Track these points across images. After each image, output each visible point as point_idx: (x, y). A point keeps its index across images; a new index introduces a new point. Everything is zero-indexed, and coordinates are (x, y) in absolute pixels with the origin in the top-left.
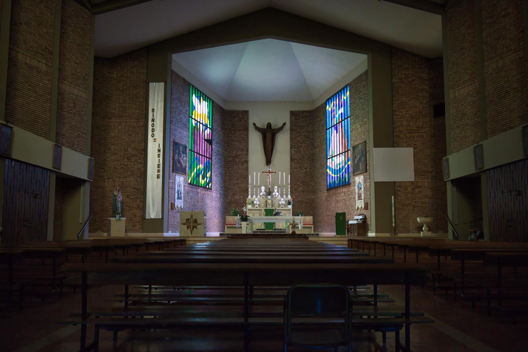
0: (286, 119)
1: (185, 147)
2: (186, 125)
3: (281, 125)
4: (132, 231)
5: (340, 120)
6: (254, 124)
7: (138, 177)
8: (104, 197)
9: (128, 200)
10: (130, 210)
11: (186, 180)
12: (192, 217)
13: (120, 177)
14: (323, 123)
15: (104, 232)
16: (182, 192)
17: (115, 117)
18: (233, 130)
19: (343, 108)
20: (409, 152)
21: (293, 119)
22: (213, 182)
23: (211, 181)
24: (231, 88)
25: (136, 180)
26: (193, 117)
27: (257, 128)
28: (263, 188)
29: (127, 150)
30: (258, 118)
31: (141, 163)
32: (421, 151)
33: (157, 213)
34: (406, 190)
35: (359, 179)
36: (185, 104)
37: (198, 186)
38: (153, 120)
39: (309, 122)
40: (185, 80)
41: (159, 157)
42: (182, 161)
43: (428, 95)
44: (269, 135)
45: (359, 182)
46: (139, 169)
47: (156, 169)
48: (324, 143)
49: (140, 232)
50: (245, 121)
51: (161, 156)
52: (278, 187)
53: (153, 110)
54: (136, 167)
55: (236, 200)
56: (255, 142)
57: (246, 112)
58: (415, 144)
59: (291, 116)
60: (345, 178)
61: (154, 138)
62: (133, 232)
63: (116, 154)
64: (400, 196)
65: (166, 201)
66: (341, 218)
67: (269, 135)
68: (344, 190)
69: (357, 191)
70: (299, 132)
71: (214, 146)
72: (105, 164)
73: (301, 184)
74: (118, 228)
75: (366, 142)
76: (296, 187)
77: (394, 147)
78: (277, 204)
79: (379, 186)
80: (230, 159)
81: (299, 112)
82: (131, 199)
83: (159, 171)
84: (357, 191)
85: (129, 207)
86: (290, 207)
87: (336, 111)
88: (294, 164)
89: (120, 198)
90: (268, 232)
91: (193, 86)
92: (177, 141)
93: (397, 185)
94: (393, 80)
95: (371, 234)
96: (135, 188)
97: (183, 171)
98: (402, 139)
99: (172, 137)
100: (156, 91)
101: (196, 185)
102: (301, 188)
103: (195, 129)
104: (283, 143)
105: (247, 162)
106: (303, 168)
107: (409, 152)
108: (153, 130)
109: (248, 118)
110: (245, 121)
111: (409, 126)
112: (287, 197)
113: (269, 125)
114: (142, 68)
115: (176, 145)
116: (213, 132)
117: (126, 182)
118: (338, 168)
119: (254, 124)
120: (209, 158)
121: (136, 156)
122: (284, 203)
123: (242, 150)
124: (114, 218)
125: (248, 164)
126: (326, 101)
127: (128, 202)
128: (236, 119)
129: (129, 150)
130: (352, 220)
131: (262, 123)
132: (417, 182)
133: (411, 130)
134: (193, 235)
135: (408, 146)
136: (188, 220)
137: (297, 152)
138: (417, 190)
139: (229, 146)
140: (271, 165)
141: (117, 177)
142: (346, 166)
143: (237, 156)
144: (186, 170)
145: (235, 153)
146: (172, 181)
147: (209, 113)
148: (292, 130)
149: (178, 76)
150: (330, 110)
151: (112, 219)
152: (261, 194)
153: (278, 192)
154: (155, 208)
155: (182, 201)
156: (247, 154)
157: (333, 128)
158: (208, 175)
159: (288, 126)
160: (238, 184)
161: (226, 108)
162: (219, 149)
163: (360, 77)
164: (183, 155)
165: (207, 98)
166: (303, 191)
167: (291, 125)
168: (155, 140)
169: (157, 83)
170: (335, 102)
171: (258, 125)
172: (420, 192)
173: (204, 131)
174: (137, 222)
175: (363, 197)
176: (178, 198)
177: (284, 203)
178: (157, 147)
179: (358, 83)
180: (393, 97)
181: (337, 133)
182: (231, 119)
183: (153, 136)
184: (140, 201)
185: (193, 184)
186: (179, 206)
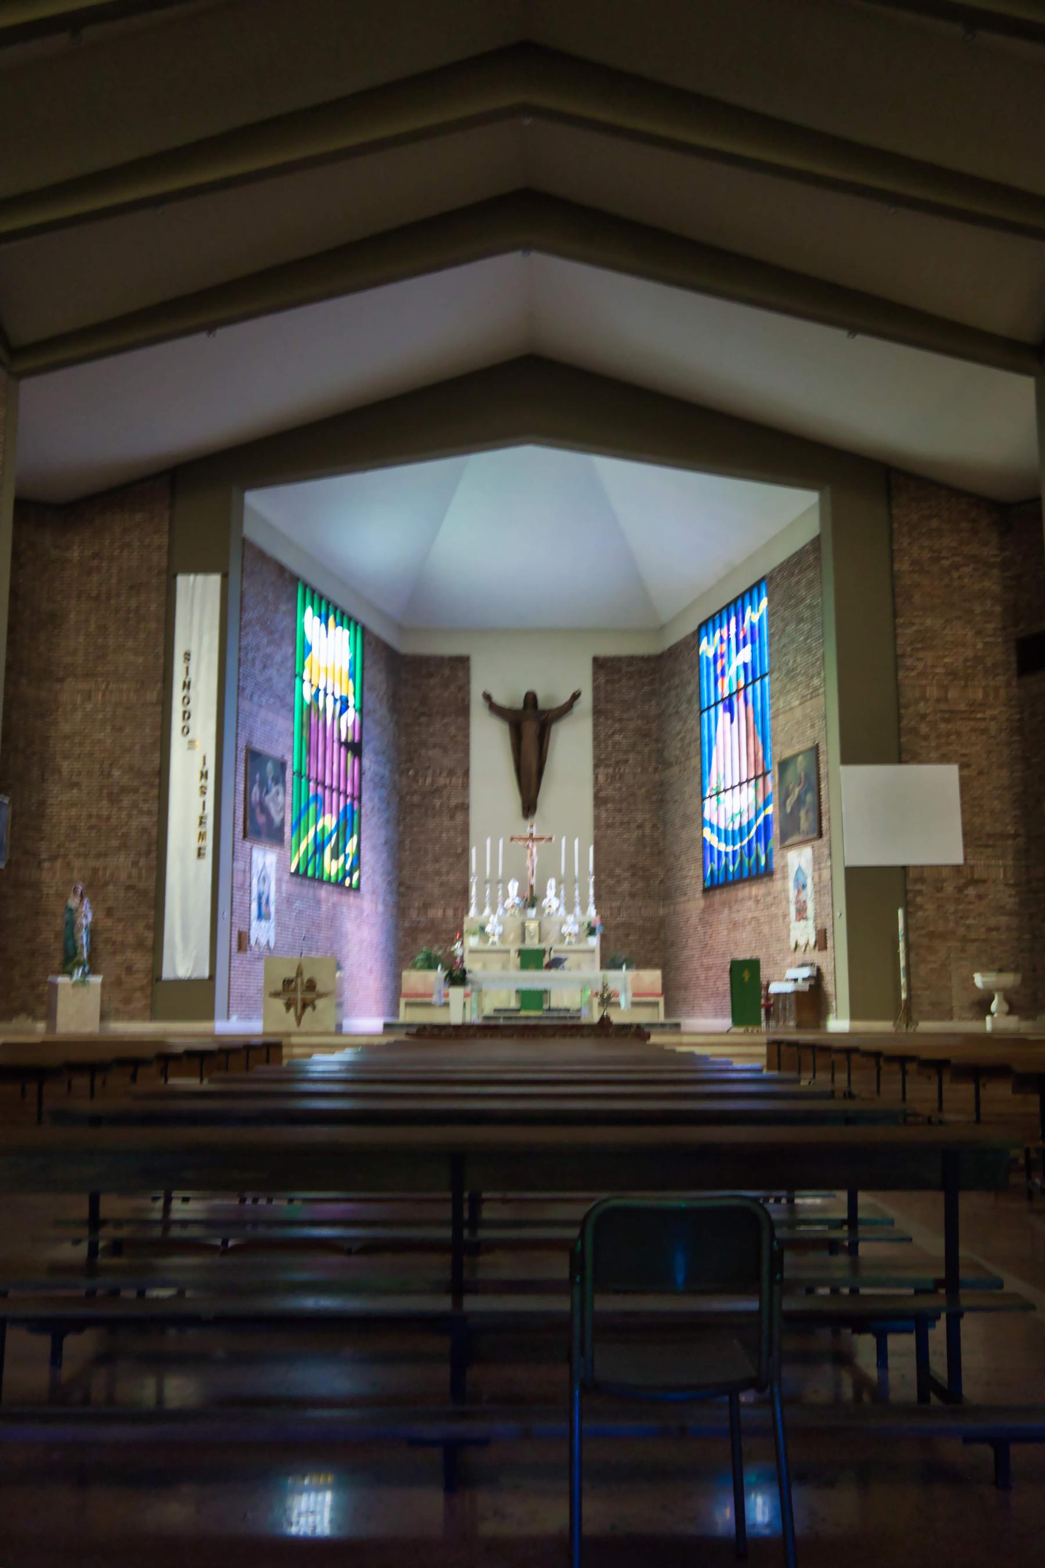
0: (582, 680)
2: (285, 701)
6: (487, 697)
9: (109, 922)
10: (114, 953)
11: (282, 864)
12: (299, 973)
15: (36, 1018)
16: (272, 898)
22: (366, 868)
24: (418, 596)
25: (135, 864)
27: (495, 709)
28: (513, 887)
29: (109, 775)
30: (499, 677)
31: (149, 813)
32: (981, 773)
34: (940, 890)
35: (798, 860)
37: (319, 880)
38: (187, 685)
40: (281, 570)
43: (998, 609)
44: (531, 727)
46: (144, 830)
47: (196, 830)
48: (698, 751)
52: (559, 883)
53: (187, 656)
54: (134, 823)
57: (462, 663)
58: (964, 755)
59: (595, 674)
61: (190, 736)
63: (76, 785)
64: (921, 907)
67: (530, 729)
69: (792, 894)
70: (620, 720)
71: (366, 762)
73: (627, 874)
74: (78, 1008)
76: (611, 882)
80: (416, 799)
83: (202, 836)
84: (792, 894)
85: (114, 943)
87: (728, 657)
88: (604, 815)
89: (86, 917)
90: (527, 1018)
91: (306, 586)
92: (258, 746)
93: (912, 874)
94: (896, 567)
96: (129, 888)
97: (274, 835)
98: (926, 738)
102: (626, 886)
103: (311, 710)
105: (465, 807)
106: (633, 825)
107: (946, 777)
108: (187, 715)
111: (946, 700)
113: (531, 699)
115: (254, 757)
117: (105, 868)
119: (487, 697)
121: (136, 791)
123: (451, 773)
129: (116, 773)
130: (780, 980)
131: (510, 696)
132: (972, 867)
133: (951, 712)
136: (287, 983)
137: (613, 777)
138: (971, 891)
141: (78, 855)
145: (429, 781)
147: (353, 663)
148: (598, 712)
149: (261, 556)
152: (509, 903)
153: (557, 895)
156: (466, 786)
158: (351, 847)
159: (586, 702)
161: (408, 647)
165: (346, 618)
166: (632, 896)
167: (596, 699)
169: (200, 578)
171: (499, 699)
172: (980, 897)
175: (810, 912)
180: (895, 615)
182: (416, 682)
183: (186, 730)
184: (148, 927)
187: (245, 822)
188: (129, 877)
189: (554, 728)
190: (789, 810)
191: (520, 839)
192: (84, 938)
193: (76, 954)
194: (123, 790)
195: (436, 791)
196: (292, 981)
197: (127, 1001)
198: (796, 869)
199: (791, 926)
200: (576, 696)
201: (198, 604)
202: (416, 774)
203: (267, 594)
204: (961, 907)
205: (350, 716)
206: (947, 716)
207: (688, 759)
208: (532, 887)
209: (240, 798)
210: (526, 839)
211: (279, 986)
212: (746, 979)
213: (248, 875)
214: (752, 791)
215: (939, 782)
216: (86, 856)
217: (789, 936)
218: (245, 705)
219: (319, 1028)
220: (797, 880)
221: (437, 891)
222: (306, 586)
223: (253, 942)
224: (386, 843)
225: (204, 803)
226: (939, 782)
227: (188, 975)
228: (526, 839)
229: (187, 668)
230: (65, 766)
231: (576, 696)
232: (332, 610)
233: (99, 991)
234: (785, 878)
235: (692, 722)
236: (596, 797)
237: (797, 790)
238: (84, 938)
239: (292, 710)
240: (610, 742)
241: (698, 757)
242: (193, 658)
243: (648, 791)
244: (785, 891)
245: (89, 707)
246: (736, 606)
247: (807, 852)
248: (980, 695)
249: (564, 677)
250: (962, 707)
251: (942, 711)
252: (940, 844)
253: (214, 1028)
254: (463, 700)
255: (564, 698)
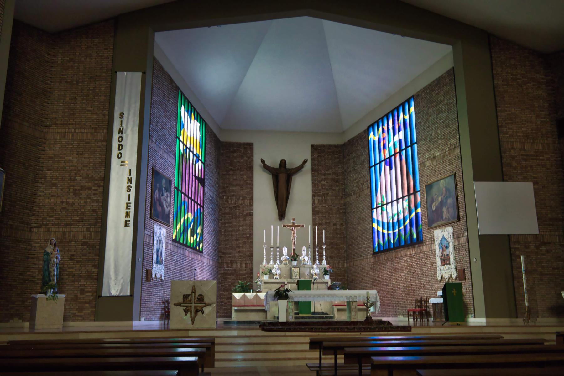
0: (307, 155)
1: (170, 182)
2: (171, 149)
3: (301, 163)
4: (75, 318)
5: (378, 161)
6: (263, 161)
7: (90, 225)
8: (28, 258)
9: (71, 263)
10: (73, 281)
11: (169, 234)
12: (193, 291)
13: (58, 225)
14: (362, 158)
15: (24, 320)
16: (164, 252)
17: (56, 124)
18: (231, 170)
19: (402, 133)
20: (525, 189)
21: (316, 155)
22: (205, 242)
23: (202, 240)
25: (88, 230)
26: (182, 139)
27: (266, 167)
28: (285, 250)
29: (75, 180)
30: (268, 153)
31: (97, 201)
32: (544, 187)
33: (122, 285)
35: (443, 234)
36: (171, 115)
37: (185, 245)
38: (121, 131)
39: (337, 160)
40: (171, 81)
41: (129, 190)
42: (164, 202)
43: (546, 105)
44: (282, 177)
45: (444, 238)
46: (94, 211)
47: (124, 211)
48: (367, 187)
49: (91, 321)
50: (249, 158)
51: (133, 190)
52: (308, 248)
53: (122, 115)
54: (88, 207)
55: (235, 270)
56: (263, 187)
57: (250, 146)
58: (535, 178)
59: (312, 152)
60: (411, 235)
61: (122, 159)
62: (77, 320)
63: (55, 185)
65: (138, 265)
66: (454, 292)
67: (282, 178)
68: (409, 252)
69: (438, 251)
70: (325, 175)
71: (206, 189)
72: (35, 202)
74: (50, 316)
75: (455, 175)
77: (503, 180)
78: (307, 273)
79: (487, 242)
80: (227, 210)
81: (323, 146)
82: (78, 262)
83: (128, 215)
84: (438, 251)
85: (74, 276)
86: (327, 278)
87: (387, 139)
89: (57, 258)
90: (303, 318)
91: (182, 94)
93: (513, 239)
94: (496, 82)
95: (477, 321)
96: (84, 243)
97: (164, 219)
99: (151, 161)
100: (127, 100)
101: (183, 244)
103: (183, 157)
104: (302, 188)
105: (251, 215)
106: (331, 224)
107: (525, 189)
108: (120, 147)
109: (252, 152)
110: (249, 158)
111: (524, 149)
112: (321, 264)
113: (283, 163)
114: (105, 49)
115: (156, 175)
116: (207, 170)
117: (70, 232)
118: (395, 220)
119: (263, 161)
120: (200, 205)
121: (90, 188)
122: (318, 271)
123: (244, 198)
124: (43, 295)
125: (252, 218)
126: (369, 127)
127: (72, 268)
128: (235, 154)
129: (78, 178)
130: (435, 297)
131: (273, 161)
132: (543, 236)
133: (527, 155)
134: (196, 326)
135: (525, 179)
136: (186, 297)
137: (322, 201)
138: (543, 248)
139: (225, 192)
140: (285, 219)
141: (53, 225)
142: (413, 214)
143: (238, 206)
144: (170, 218)
146: (149, 233)
147: (201, 139)
148: (314, 170)
149: (162, 69)
150: (376, 139)
151: (39, 296)
152: (283, 258)
153: (307, 255)
154: (119, 278)
155: (163, 267)
156: (251, 204)
157: (383, 163)
158: (199, 231)
159: (308, 166)
160: (238, 246)
161: (224, 138)
162: (212, 195)
163: (437, 83)
164: (165, 194)
165: (199, 117)
167: (313, 164)
168: (123, 163)
169: (130, 74)
170: (385, 128)
171: (268, 163)
172: (548, 251)
173: (194, 164)
174: (86, 303)
175: (452, 259)
176: (157, 263)
177: (318, 271)
178: (126, 176)
179: (434, 91)
181: (391, 169)
182: (228, 155)
184: (93, 266)
185: (179, 242)
186: (159, 276)
187: (151, 210)
188: (84, 238)
189: (293, 177)
190: (434, 209)
191: (288, 226)
192: (54, 271)
193: (50, 280)
194: (83, 188)
195: (237, 207)
196: (189, 295)
197: (80, 309)
198: (440, 238)
199: (438, 268)
200: (305, 162)
201: (128, 87)
202: (228, 198)
203: (166, 92)
204: (539, 256)
205: (199, 165)
206: (525, 157)
207: (362, 190)
208: (294, 250)
209: (149, 195)
210: (290, 226)
211: (181, 300)
212: (455, 294)
213: (152, 238)
214: (406, 204)
215: (523, 191)
216: (58, 225)
217: (436, 273)
218: (153, 145)
219: (205, 326)
220: (441, 244)
221: (237, 255)
222: (182, 94)
223: (154, 276)
224: (214, 230)
225: (129, 195)
226: (523, 191)
227: (117, 294)
228: (290, 226)
229: (122, 121)
230: (49, 174)
231: (305, 162)
232: (193, 111)
233: (63, 303)
234: (432, 243)
235: (364, 172)
236: (314, 211)
237: (440, 199)
238: (54, 271)
239: (175, 155)
240: (320, 185)
241: (369, 190)
242: (125, 116)
243: (338, 208)
244: (433, 251)
245: (64, 141)
246: (393, 113)
247: (450, 229)
248: (541, 147)
249: (298, 154)
250: (532, 153)
251: (522, 155)
252: (525, 223)
253: (132, 326)
254: (250, 163)
255: (299, 163)
